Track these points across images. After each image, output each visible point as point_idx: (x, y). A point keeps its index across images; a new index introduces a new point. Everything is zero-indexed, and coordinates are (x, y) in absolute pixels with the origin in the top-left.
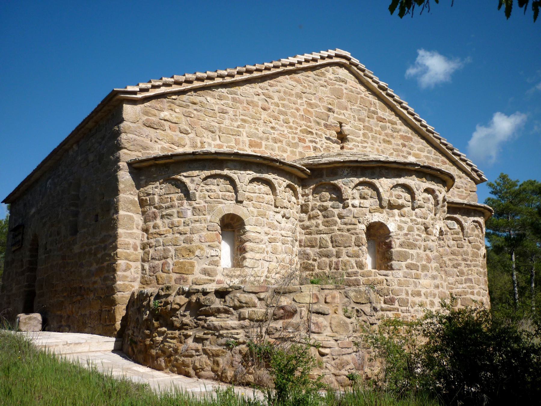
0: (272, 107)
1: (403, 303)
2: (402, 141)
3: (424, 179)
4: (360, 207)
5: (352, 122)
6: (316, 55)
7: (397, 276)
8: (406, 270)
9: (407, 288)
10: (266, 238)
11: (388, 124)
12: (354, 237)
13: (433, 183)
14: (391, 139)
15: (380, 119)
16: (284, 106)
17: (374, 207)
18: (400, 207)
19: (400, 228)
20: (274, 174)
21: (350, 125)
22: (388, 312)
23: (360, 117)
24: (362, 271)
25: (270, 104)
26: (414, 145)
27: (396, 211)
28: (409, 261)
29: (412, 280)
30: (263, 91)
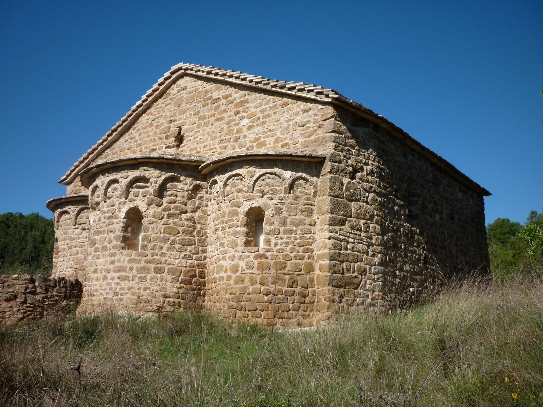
6: (155, 86)
10: (66, 247)
13: (115, 173)
20: (69, 206)
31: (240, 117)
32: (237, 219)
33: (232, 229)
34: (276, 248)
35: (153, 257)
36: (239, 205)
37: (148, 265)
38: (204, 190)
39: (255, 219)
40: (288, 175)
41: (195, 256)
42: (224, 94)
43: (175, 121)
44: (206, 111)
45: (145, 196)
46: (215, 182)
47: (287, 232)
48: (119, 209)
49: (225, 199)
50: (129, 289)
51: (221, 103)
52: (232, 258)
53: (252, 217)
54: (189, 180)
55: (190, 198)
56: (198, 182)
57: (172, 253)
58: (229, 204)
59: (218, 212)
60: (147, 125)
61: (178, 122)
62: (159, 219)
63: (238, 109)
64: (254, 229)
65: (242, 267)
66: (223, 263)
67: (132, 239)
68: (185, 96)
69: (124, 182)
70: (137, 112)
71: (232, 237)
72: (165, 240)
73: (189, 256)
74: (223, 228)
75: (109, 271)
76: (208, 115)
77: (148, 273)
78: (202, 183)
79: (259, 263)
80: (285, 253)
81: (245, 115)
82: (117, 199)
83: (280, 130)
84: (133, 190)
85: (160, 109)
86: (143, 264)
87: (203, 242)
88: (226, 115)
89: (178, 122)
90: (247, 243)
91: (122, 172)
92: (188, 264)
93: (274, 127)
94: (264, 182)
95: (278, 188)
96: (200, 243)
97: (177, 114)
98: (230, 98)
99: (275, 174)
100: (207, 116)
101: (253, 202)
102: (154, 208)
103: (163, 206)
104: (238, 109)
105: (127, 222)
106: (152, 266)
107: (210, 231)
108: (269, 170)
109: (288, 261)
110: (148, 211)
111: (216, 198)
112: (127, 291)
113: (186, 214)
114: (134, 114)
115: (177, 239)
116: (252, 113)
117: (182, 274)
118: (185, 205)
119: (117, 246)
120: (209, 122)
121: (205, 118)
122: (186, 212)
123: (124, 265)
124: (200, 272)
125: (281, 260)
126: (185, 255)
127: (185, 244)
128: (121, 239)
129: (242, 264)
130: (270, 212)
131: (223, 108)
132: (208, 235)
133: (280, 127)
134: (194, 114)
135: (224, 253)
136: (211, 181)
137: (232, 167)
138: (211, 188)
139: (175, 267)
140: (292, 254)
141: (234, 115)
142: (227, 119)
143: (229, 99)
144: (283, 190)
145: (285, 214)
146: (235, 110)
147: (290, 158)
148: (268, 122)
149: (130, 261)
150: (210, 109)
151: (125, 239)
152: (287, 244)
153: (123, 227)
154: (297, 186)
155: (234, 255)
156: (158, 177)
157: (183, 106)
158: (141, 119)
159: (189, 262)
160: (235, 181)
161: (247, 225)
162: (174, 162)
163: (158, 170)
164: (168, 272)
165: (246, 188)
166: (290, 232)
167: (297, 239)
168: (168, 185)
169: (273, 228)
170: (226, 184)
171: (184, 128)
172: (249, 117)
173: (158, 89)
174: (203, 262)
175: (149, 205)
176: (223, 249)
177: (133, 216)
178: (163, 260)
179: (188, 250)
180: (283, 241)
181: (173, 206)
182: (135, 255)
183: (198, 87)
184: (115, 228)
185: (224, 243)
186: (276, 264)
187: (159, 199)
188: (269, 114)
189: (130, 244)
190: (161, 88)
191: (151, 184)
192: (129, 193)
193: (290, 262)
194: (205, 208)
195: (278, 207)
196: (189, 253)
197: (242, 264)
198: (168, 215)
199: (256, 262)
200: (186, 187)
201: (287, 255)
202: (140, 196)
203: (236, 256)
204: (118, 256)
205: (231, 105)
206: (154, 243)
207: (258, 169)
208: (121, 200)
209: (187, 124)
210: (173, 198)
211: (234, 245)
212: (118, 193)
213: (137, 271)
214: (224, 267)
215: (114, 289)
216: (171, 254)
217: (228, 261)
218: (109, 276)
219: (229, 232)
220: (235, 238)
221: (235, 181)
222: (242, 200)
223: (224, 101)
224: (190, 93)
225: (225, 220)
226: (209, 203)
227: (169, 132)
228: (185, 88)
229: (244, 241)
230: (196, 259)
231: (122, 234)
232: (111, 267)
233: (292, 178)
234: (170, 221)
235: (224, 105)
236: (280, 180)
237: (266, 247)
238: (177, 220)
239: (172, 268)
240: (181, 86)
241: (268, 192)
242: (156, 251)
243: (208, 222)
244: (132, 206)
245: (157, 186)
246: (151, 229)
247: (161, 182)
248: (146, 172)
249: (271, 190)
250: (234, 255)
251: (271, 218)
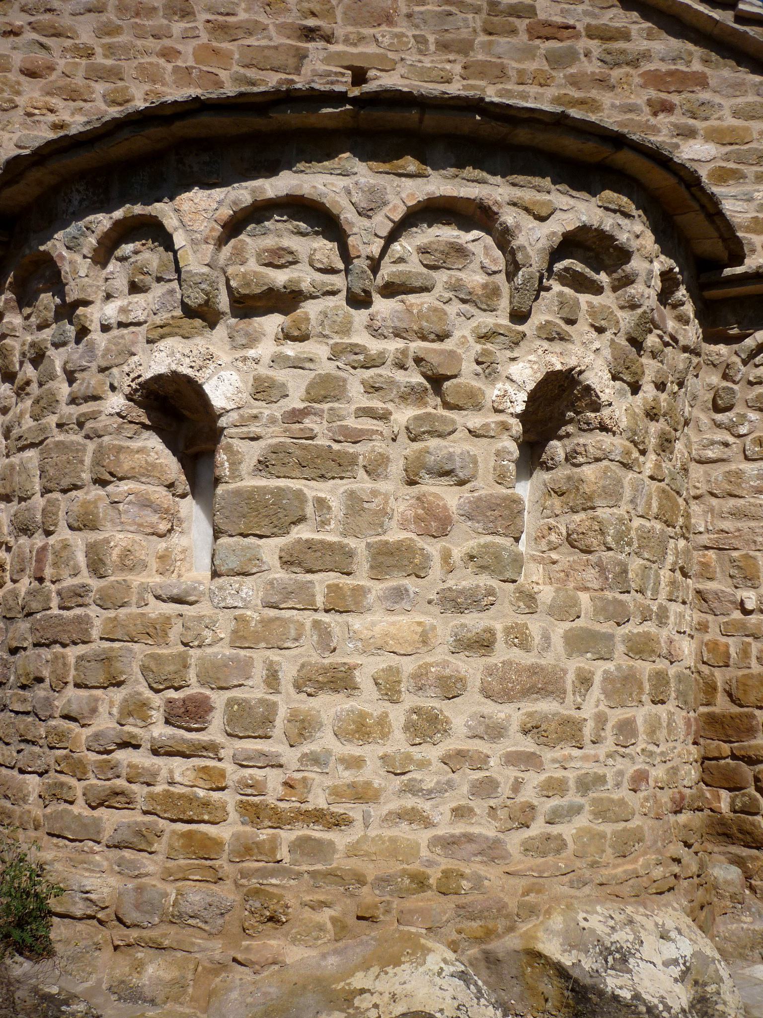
0: (61, 64)
1: (251, 722)
2: (653, 93)
3: (411, 164)
4: (121, 325)
5: (412, 57)
7: (230, 602)
8: (280, 574)
9: (274, 656)
11: (584, 43)
12: (91, 446)
14: (594, 93)
15: (547, 31)
16: (110, 50)
17: (163, 317)
18: (285, 300)
19: (264, 390)
21: (401, 69)
22: (177, 762)
23: (448, 36)
24: (102, 583)
25: (56, 53)
26: (717, 99)
27: (272, 323)
28: (303, 533)
29: (307, 618)
30: (32, 19)
35: (140, 610)
50: (585, 785)
75: (451, 688)
112: (579, 800)
119: (497, 557)
123: (547, 660)
215: (505, 790)
218: (460, 715)
227: (298, 70)
232: (471, 668)
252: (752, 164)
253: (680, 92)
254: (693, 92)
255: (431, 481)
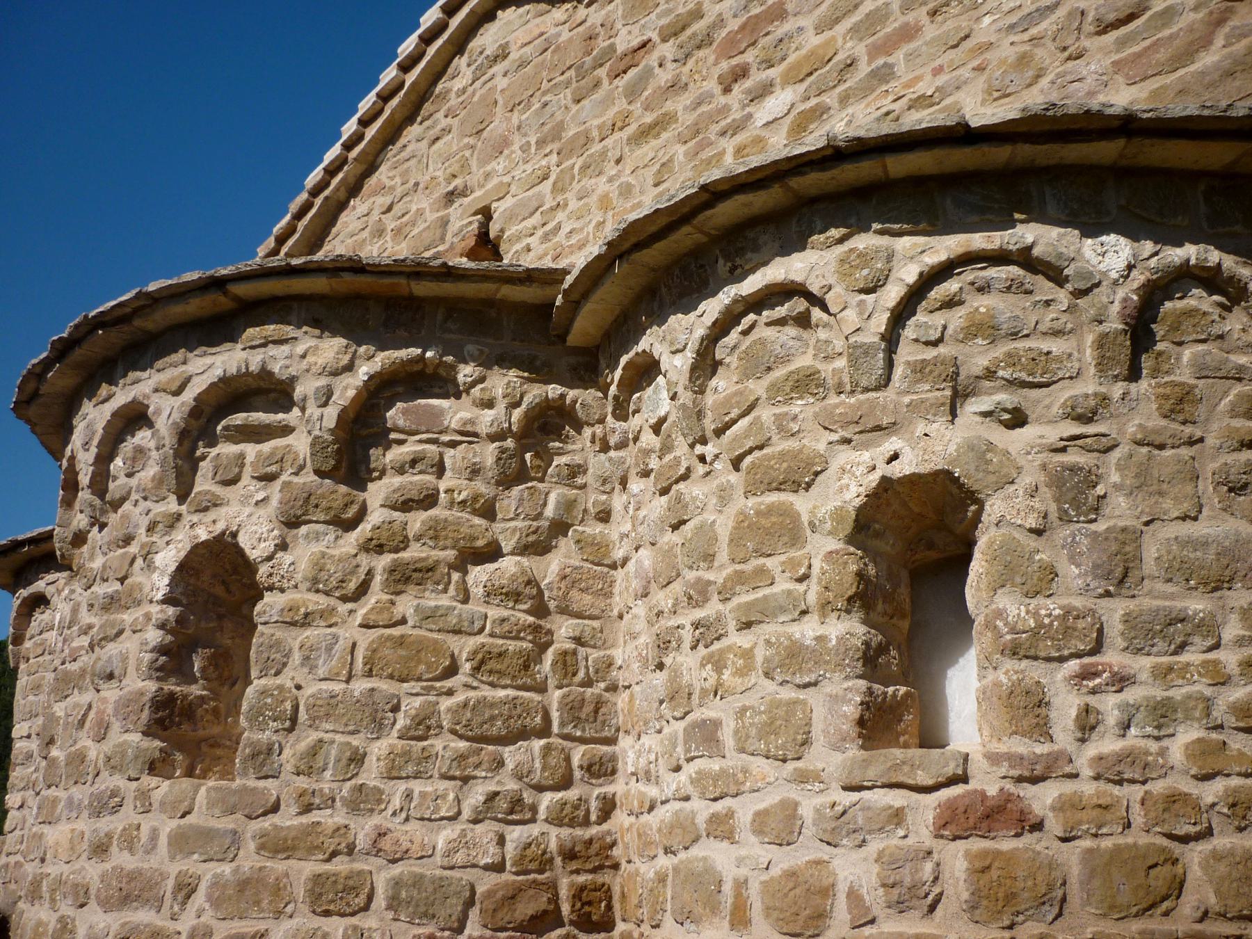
6: (390, 74)
13: (133, 375)
20: (47, 572)
31: (748, 91)
32: (793, 564)
33: (768, 630)
34: (1095, 748)
35: (306, 819)
36: (802, 476)
37: (278, 866)
38: (587, 432)
39: (915, 557)
40: (1111, 255)
41: (547, 800)
42: (664, 21)
43: (463, 194)
44: (591, 115)
45: (269, 478)
46: (647, 370)
47: (1150, 634)
48: (148, 554)
49: (709, 450)
51: (652, 59)
52: (781, 826)
53: (886, 546)
54: (501, 382)
55: (512, 476)
56: (554, 390)
57: (417, 786)
58: (734, 478)
59: (670, 538)
60: (365, 234)
61: (478, 193)
62: (344, 599)
63: (734, 61)
64: (905, 625)
65: (854, 896)
66: (717, 854)
67: (216, 711)
68: (501, 83)
69: (169, 412)
70: (327, 192)
71: (770, 686)
72: (376, 716)
73: (516, 803)
74: (707, 632)
76: (600, 127)
77: (278, 914)
78: (572, 394)
79: (981, 868)
80: (1158, 787)
81: (773, 73)
82: (143, 505)
83: (981, 82)
84: (214, 452)
85: (413, 162)
86: (249, 859)
87: (592, 718)
88: (678, 104)
89: (478, 193)
90: (876, 725)
91: (159, 364)
92: (510, 848)
93: (941, 80)
94: (956, 319)
95: (1056, 346)
96: (577, 721)
97: (474, 163)
98: (698, 27)
99: (1025, 258)
100: (595, 134)
101: (893, 443)
102: (317, 537)
103: (365, 529)
104: (734, 61)
105: (180, 620)
106: (304, 869)
107: (627, 651)
108: (979, 241)
109: (1185, 839)
110: (286, 558)
111: (654, 463)
113: (490, 567)
114: (318, 201)
115: (446, 703)
116: (812, 53)
117: (474, 914)
118: (489, 512)
120: (604, 153)
121: (589, 139)
122: (492, 553)
124: (579, 893)
125: (1138, 838)
126: (492, 797)
127: (490, 733)
128: (145, 715)
129: (854, 869)
130: (1021, 501)
131: (663, 77)
132: (622, 678)
133: (980, 69)
134: (541, 143)
135: (723, 788)
136: (618, 373)
137: (741, 252)
138: (622, 412)
139: (431, 869)
140: (1211, 792)
141: (717, 90)
142: (686, 119)
143: (689, 32)
144: (1089, 354)
145: (1121, 510)
146: (725, 65)
147: (1106, 151)
148: (900, 69)
149: (182, 843)
150: (609, 100)
151: (167, 717)
152: (1163, 715)
153: (162, 650)
154: (1175, 328)
155: (790, 810)
156: (336, 373)
157: (497, 126)
158: (344, 218)
159: (516, 835)
160: (762, 332)
161: (864, 598)
162: (422, 289)
163: (334, 334)
164: (394, 904)
165: (841, 363)
166: (1169, 631)
167: (1223, 681)
168: (395, 415)
169: (1051, 607)
170: (706, 364)
171: (499, 209)
172: (793, 78)
173: (396, 88)
174: (594, 830)
175: (292, 523)
176: (715, 765)
177: (219, 591)
178: (363, 830)
179: (510, 765)
180: (1132, 695)
181: (417, 521)
182: (211, 805)
183: (553, 31)
184: (124, 658)
185: (717, 724)
186: (1097, 865)
187: (343, 489)
188: (906, 25)
189: (199, 742)
190: (411, 78)
191: (303, 410)
192: (195, 469)
193: (1203, 847)
194: (594, 529)
195: (1074, 469)
196: (512, 785)
197: (854, 869)
198: (392, 571)
199: (956, 859)
200: (487, 420)
201: (1174, 799)
202: (246, 479)
203: (806, 811)
204: (128, 815)
205: (701, 53)
206: (314, 736)
207: (906, 241)
208: (159, 508)
209: (513, 189)
210: (418, 480)
211: (787, 739)
212: (150, 471)
213: (216, 902)
214: (727, 888)
216: (409, 796)
217: (755, 849)
219: (748, 654)
220: (788, 694)
221: (770, 333)
222: (819, 442)
223: (668, 50)
224: (523, 64)
225: (717, 576)
226: (618, 502)
227: (442, 239)
228: (502, 54)
229: (851, 710)
230: (558, 818)
231: (152, 686)
232: (92, 872)
233: (1139, 278)
234: (406, 605)
235: (670, 66)
236: (1063, 297)
237: (1020, 746)
238: (444, 601)
239: (418, 881)
240: (488, 52)
241: (990, 374)
242: (326, 784)
243: (618, 603)
244: (203, 535)
245: (331, 415)
246: (297, 657)
247: (351, 393)
248: (272, 350)
249: (1012, 360)
250: (790, 810)
251: (1032, 542)
252: (835, 86)
253: (753, 44)
254: (767, 34)
255: (106, 686)
